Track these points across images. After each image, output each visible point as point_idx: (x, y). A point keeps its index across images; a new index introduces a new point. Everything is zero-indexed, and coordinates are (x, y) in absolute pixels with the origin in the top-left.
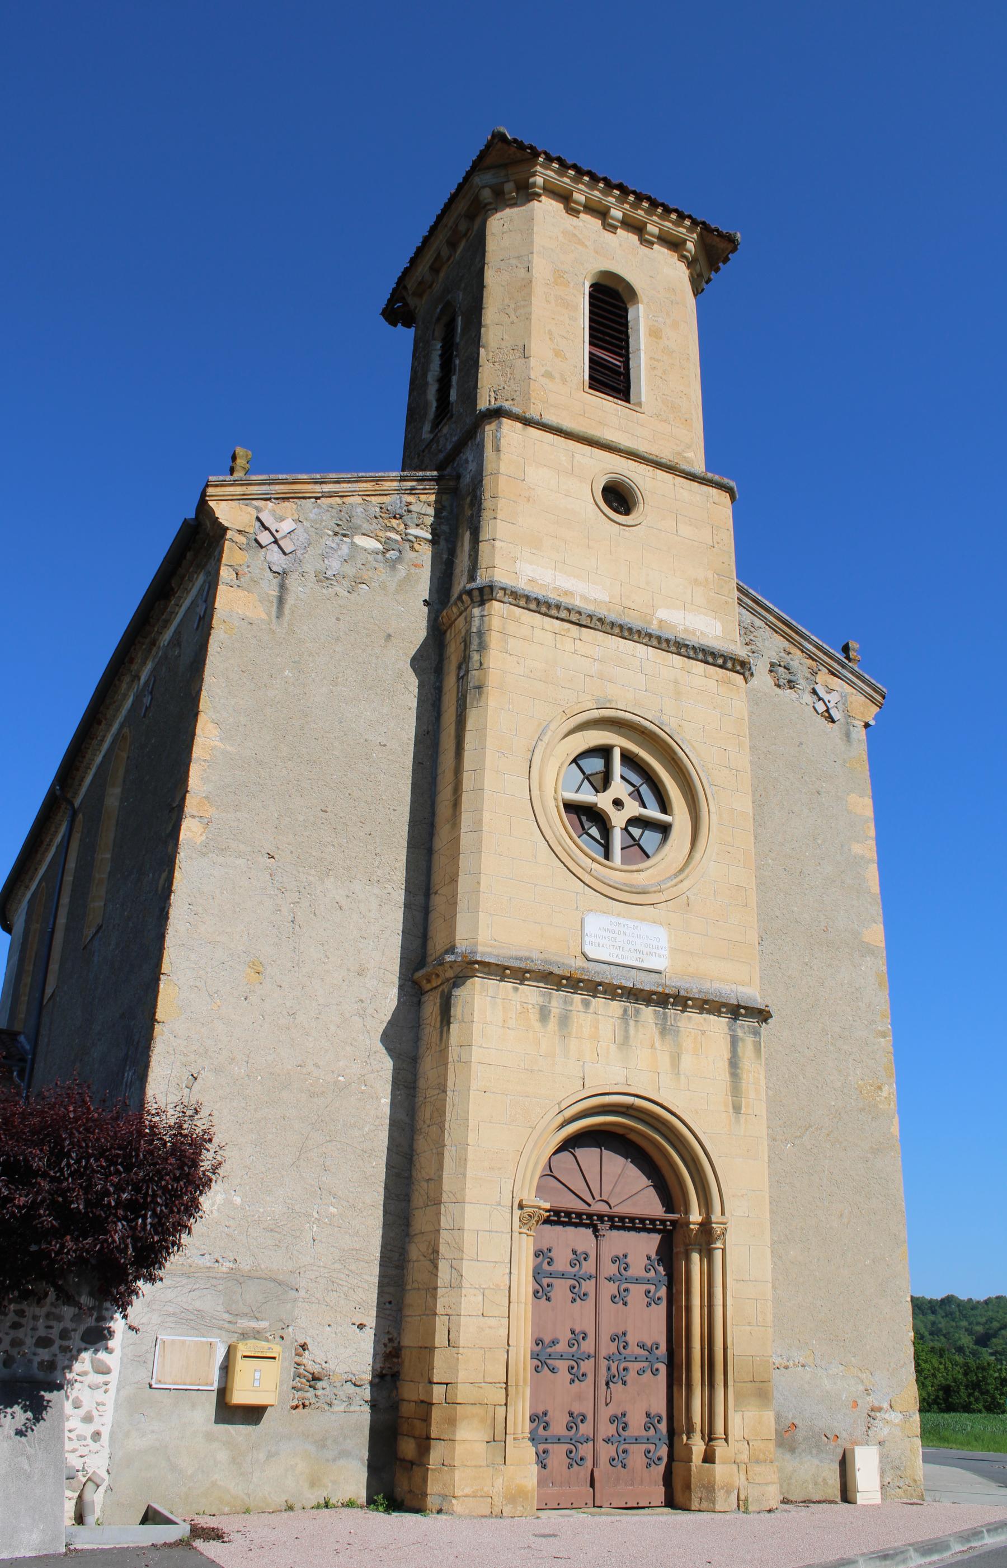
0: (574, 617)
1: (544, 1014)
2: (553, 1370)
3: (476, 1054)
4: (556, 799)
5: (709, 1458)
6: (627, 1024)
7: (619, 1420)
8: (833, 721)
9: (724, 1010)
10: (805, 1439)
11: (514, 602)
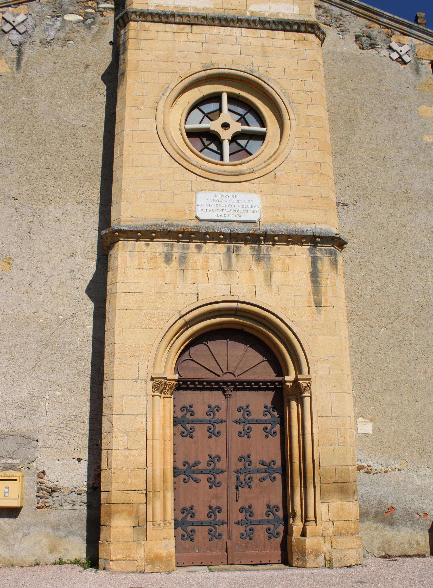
0: (185, 20)
1: (168, 258)
2: (196, 481)
3: (120, 287)
4: (180, 130)
5: (304, 534)
6: (230, 257)
7: (248, 510)
8: (405, 63)
9: (304, 240)
10: (401, 516)
11: (144, 19)
